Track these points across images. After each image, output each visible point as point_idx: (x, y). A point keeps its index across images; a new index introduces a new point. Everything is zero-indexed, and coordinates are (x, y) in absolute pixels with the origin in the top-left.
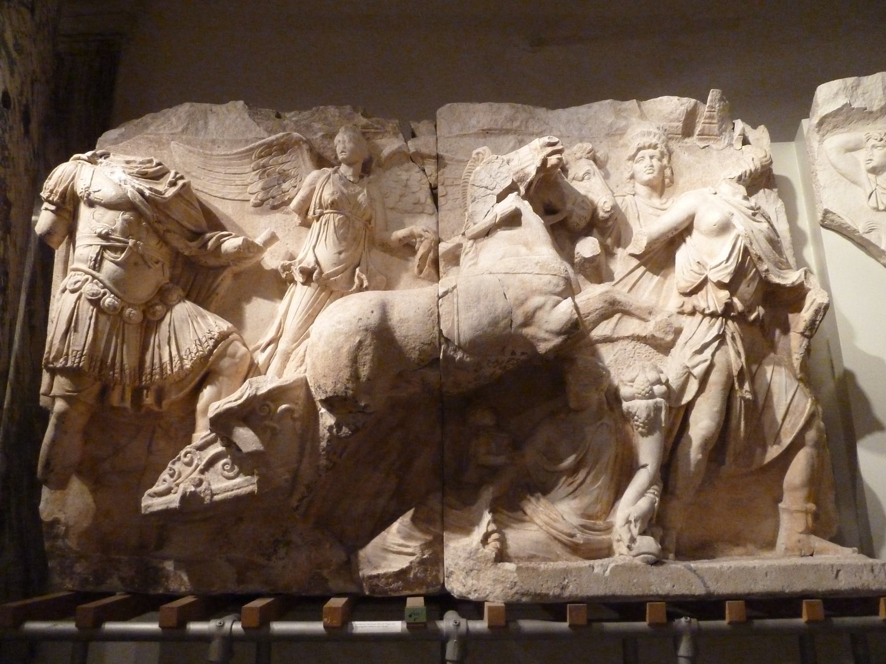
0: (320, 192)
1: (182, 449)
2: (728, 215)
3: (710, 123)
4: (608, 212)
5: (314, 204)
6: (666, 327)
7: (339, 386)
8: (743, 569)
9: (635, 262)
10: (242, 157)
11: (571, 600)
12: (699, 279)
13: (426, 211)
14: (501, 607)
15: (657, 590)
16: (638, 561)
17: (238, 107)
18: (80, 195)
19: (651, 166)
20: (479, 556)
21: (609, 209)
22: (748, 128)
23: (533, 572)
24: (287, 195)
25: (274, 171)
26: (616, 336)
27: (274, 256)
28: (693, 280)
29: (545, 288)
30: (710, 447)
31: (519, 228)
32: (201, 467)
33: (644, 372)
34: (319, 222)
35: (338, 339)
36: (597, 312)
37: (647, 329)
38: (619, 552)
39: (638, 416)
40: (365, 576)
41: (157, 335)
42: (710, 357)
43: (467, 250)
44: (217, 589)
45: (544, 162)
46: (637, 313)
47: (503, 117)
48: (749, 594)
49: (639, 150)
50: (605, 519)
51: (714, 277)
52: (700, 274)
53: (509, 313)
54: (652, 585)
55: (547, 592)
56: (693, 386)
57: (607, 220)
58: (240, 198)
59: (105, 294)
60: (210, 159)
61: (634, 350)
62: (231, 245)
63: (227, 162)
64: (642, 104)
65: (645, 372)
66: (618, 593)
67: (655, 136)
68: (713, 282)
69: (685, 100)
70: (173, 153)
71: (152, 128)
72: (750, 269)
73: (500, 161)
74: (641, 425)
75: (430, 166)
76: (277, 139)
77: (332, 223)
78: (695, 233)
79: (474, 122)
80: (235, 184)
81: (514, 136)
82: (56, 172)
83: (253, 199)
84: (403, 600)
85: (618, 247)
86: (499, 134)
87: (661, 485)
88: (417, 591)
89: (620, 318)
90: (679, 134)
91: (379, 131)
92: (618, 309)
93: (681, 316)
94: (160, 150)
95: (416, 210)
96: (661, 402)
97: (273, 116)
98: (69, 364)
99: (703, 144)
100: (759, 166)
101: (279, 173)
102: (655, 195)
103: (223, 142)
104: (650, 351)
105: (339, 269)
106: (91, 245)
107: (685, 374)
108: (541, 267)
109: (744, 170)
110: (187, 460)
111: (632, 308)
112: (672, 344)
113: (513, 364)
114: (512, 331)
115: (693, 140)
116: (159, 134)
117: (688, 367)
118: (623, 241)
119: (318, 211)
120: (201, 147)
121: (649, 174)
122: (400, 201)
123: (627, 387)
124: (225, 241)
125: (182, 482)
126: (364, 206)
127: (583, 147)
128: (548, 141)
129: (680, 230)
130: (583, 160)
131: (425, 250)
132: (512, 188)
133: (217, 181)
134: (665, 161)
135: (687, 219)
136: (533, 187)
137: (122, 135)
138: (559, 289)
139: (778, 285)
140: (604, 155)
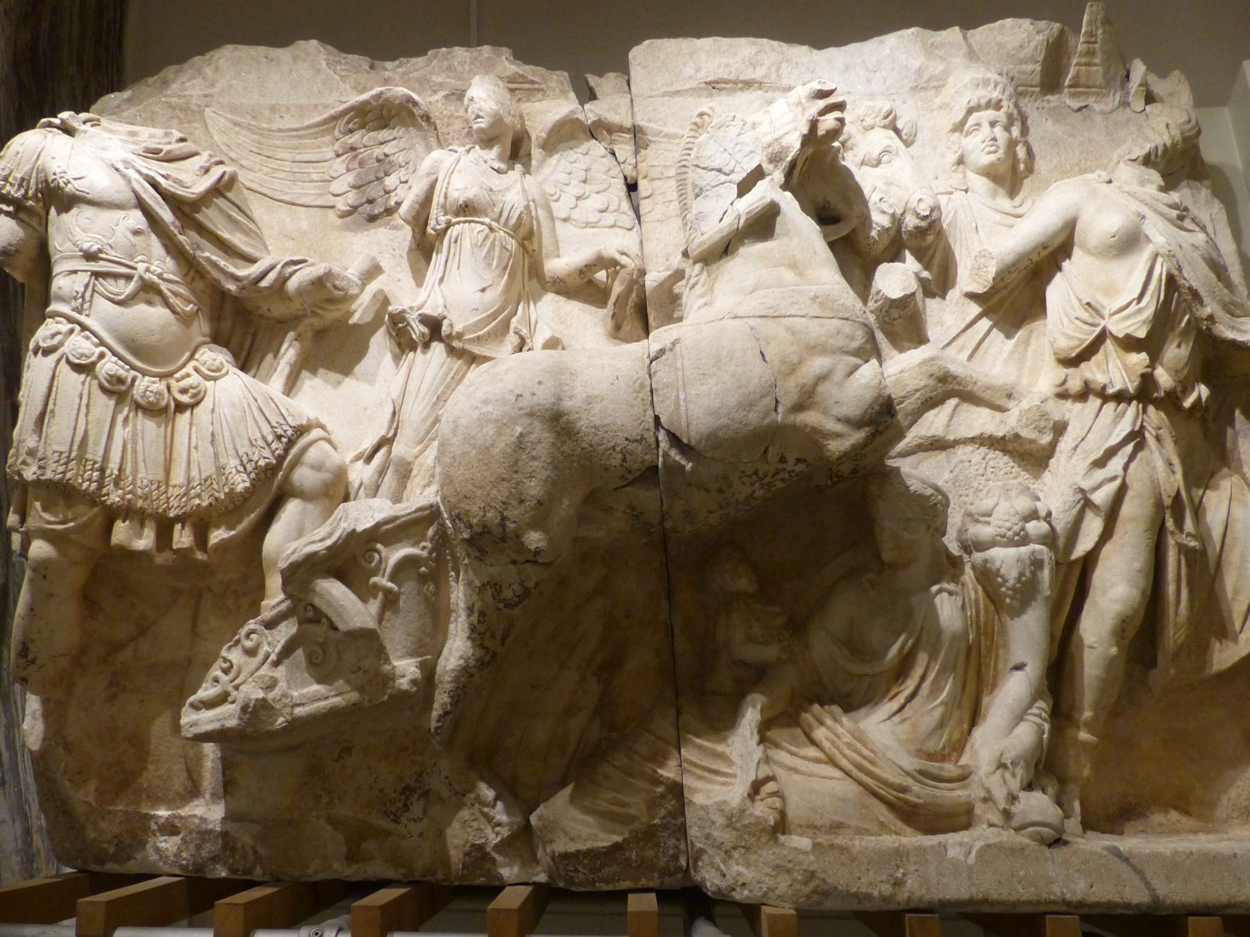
1: (242, 626)
2: (1135, 218)
3: (1088, 65)
6: (1040, 420)
8: (1215, 857)
9: (975, 309)
10: (317, 133)
11: (912, 905)
12: (1090, 334)
14: (791, 915)
15: (1062, 892)
16: (1022, 839)
20: (746, 822)
22: (1152, 78)
23: (842, 854)
26: (951, 437)
29: (831, 341)
30: (1130, 634)
32: (273, 657)
33: (1009, 499)
36: (918, 395)
38: (988, 821)
40: (735, 812)
42: (1121, 472)
43: (692, 281)
44: (315, 871)
45: (814, 125)
46: (986, 395)
48: (1227, 906)
49: (970, 111)
50: (957, 761)
51: (1119, 328)
52: (1092, 325)
53: (771, 386)
54: (1053, 883)
55: (870, 890)
56: (1093, 527)
58: (318, 203)
59: (102, 356)
63: (295, 142)
64: (969, 35)
65: (1010, 498)
66: (995, 896)
67: (996, 87)
68: (1115, 338)
69: (1042, 24)
71: (174, 86)
72: (1179, 316)
75: (623, 146)
77: (468, 240)
78: (1077, 252)
79: (689, 70)
83: (342, 205)
84: (622, 896)
86: (733, 91)
87: (1051, 702)
88: (643, 882)
89: (957, 406)
92: (953, 390)
94: (189, 123)
96: (1041, 552)
99: (1076, 104)
100: (1178, 137)
102: (1001, 191)
103: (288, 109)
106: (75, 272)
107: (1078, 502)
108: (822, 305)
109: (1153, 145)
110: (248, 644)
112: (1051, 450)
113: (783, 480)
114: (779, 419)
117: (1082, 491)
120: (254, 117)
121: (990, 153)
122: (577, 206)
124: (295, 271)
125: (243, 683)
126: (518, 212)
127: (875, 107)
128: (819, 87)
129: (1050, 249)
131: (622, 288)
133: (282, 175)
134: (1016, 131)
135: (1063, 228)
136: (796, 172)
137: (129, 100)
138: (855, 345)
139: (1233, 343)
140: (910, 124)
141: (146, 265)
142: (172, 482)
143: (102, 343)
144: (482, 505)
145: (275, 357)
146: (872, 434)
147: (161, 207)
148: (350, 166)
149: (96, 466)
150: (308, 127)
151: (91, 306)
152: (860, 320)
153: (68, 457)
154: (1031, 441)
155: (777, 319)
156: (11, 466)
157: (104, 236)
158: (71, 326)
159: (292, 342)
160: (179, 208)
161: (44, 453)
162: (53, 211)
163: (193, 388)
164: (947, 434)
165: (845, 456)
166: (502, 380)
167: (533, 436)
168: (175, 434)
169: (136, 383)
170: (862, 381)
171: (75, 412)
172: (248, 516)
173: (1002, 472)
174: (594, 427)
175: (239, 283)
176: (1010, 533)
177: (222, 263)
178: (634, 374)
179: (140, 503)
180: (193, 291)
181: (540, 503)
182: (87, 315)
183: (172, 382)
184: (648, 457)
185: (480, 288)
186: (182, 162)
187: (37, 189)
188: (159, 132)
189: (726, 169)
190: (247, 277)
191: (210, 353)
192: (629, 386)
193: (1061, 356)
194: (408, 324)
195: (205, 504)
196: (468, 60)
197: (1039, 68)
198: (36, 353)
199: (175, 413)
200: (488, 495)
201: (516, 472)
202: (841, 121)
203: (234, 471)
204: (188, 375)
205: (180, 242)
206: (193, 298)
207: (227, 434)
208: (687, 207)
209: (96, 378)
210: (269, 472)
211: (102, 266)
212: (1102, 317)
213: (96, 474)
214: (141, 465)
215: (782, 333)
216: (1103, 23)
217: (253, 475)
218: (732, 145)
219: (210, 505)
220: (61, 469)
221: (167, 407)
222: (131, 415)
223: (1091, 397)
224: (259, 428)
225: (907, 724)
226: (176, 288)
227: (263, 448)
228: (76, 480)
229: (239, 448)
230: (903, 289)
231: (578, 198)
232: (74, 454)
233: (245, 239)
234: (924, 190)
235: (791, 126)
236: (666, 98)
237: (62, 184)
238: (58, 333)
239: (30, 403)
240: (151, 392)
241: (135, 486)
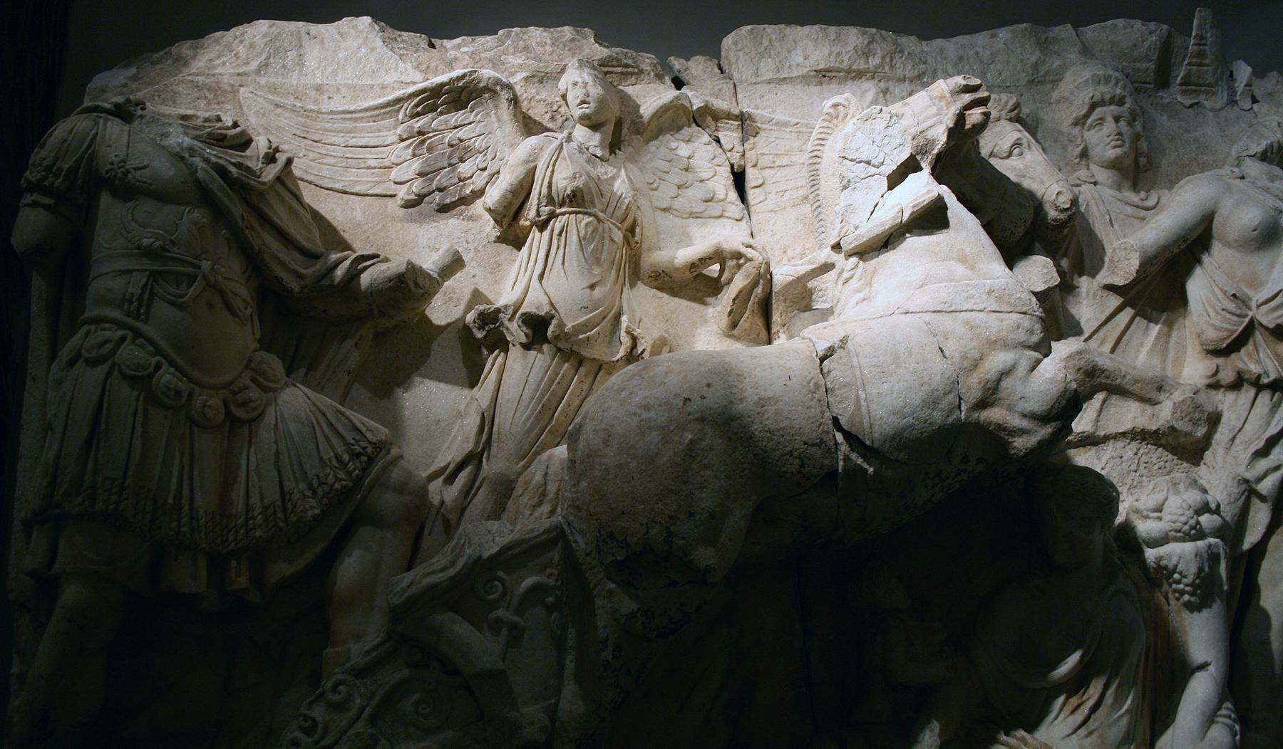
0: (548, 173)
3: (1199, 65)
4: (1066, 210)
5: (537, 196)
6: (1194, 412)
7: (655, 531)
9: (1114, 301)
10: (378, 115)
12: (1240, 325)
13: (726, 214)
17: (361, 27)
18: (107, 176)
19: (1118, 134)
21: (1068, 206)
24: (469, 185)
25: (441, 141)
26: (1102, 433)
27: (450, 299)
28: (1230, 327)
29: (1011, 336)
31: (946, 231)
33: (1177, 492)
34: (546, 233)
35: (647, 439)
37: (1163, 414)
39: (1180, 573)
41: (252, 450)
43: (846, 275)
45: (960, 118)
46: (1136, 389)
47: (851, 48)
49: (1093, 106)
52: (1239, 316)
53: (953, 383)
57: (1061, 225)
60: (315, 120)
61: (1137, 457)
62: (382, 276)
63: (349, 125)
65: (1179, 492)
68: (1266, 328)
69: (1152, 25)
70: (245, 109)
73: (885, 115)
74: (1188, 589)
75: (730, 133)
76: (451, 81)
77: (575, 231)
78: (1217, 247)
79: (797, 58)
81: (872, 82)
82: (56, 133)
83: (403, 193)
85: (1080, 276)
86: (846, 79)
89: (1104, 401)
90: (1149, 83)
91: (630, 70)
93: (1213, 392)
94: (218, 104)
95: (707, 209)
97: (424, 44)
98: (99, 506)
101: (451, 146)
102: (1127, 184)
103: (338, 90)
104: (1165, 459)
105: (594, 316)
107: (1243, 494)
108: (998, 299)
109: (1269, 142)
110: (336, 698)
111: (1125, 380)
112: (1206, 443)
115: (1175, 95)
116: (213, 75)
117: (1246, 481)
118: (1087, 263)
119: (546, 210)
123: (1149, 521)
124: (366, 268)
126: (627, 201)
128: (964, 82)
129: (1189, 242)
130: (1003, 122)
131: (746, 282)
132: (910, 166)
134: (1138, 127)
138: (1035, 338)
143: (159, 351)
144: (645, 521)
146: (1058, 429)
148: (417, 152)
150: (366, 110)
152: (1037, 313)
154: (1187, 434)
155: (953, 314)
158: (120, 333)
164: (1096, 430)
165: (1032, 452)
166: (663, 383)
167: (704, 443)
170: (1047, 375)
173: (1156, 467)
174: (769, 431)
176: (1186, 527)
178: (807, 374)
181: (712, 516)
184: (827, 462)
185: (588, 284)
189: (875, 162)
192: (804, 387)
193: (1210, 348)
194: (502, 324)
196: (549, 41)
197: (1153, 67)
200: (653, 509)
201: (685, 483)
202: (987, 115)
208: (820, 198)
212: (1250, 309)
215: (960, 329)
216: (1211, 28)
218: (880, 137)
220: (114, 498)
223: (1246, 385)
224: (331, 446)
225: (1095, 736)
230: (1046, 282)
231: (679, 187)
234: (1061, 183)
235: (935, 119)
236: (772, 85)
238: (107, 341)
240: (210, 406)
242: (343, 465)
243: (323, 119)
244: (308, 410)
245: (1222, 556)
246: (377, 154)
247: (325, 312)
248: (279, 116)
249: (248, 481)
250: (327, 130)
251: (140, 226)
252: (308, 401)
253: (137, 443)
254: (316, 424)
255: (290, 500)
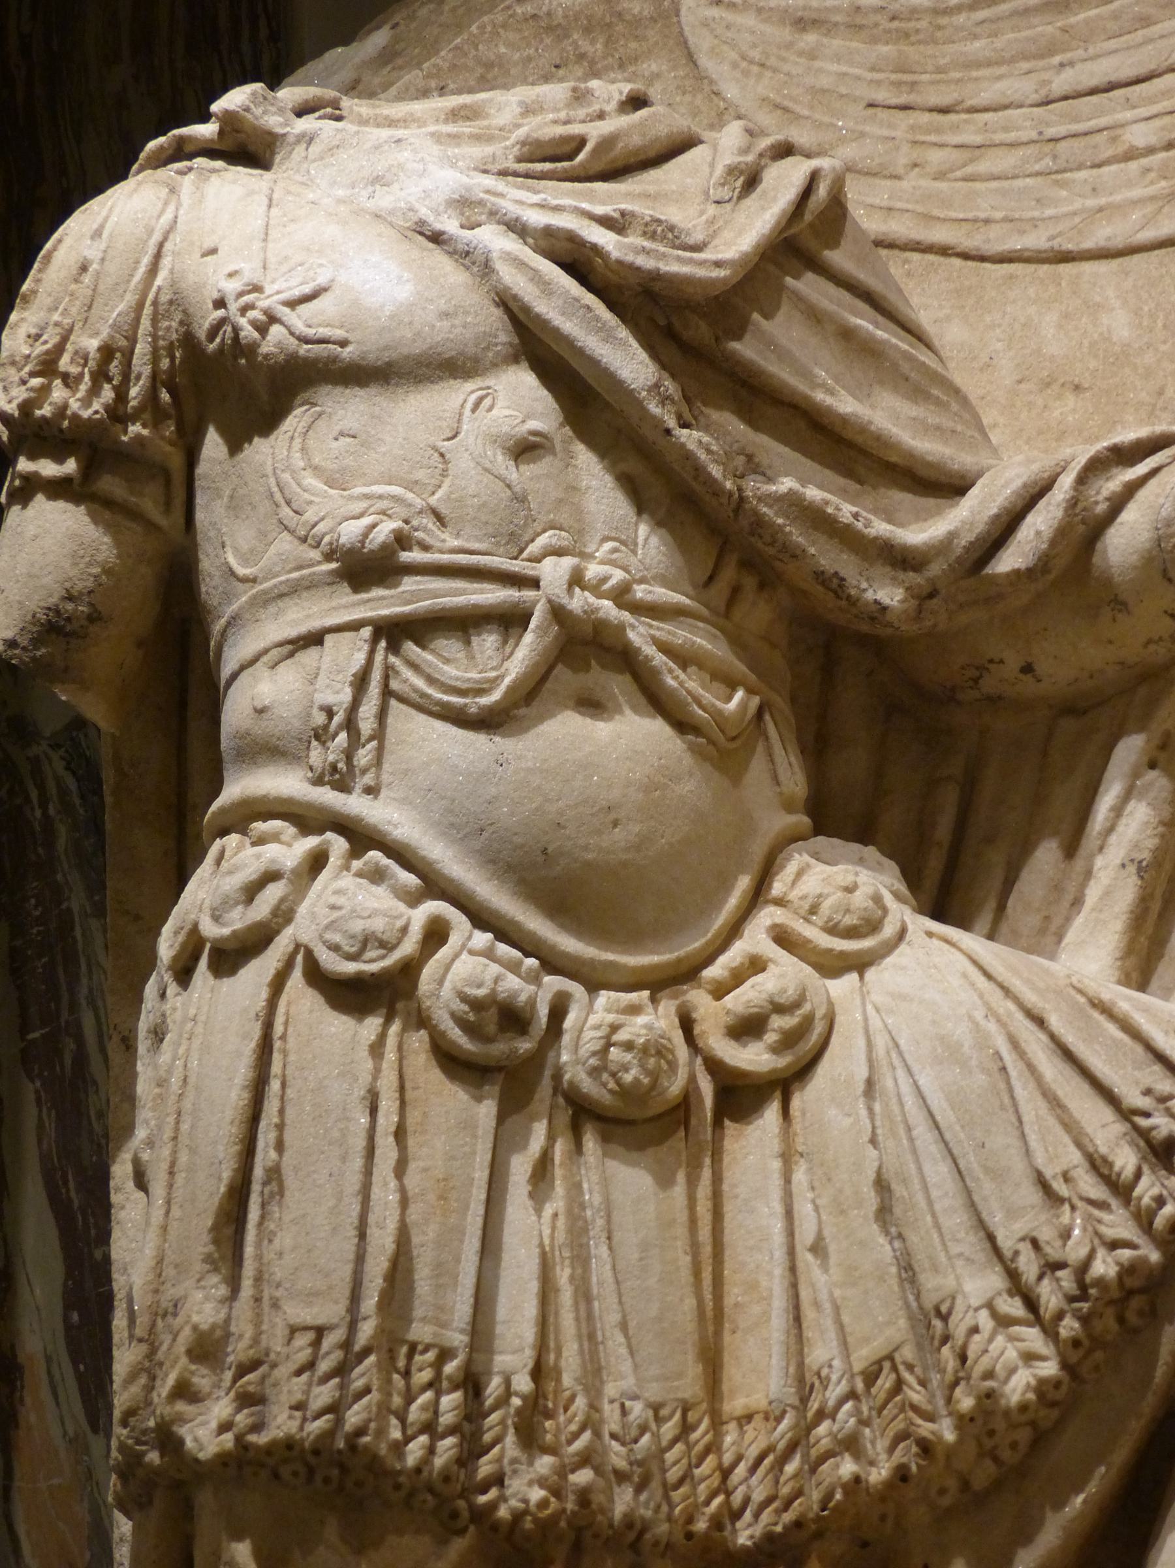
18: (212, 347)
41: (800, 1176)
59: (436, 934)
80: (1120, 149)
106: (315, 639)
124: (1131, 489)
141: (568, 562)
142: (735, 1405)
145: (1071, 849)
147: (608, 336)
149: (450, 1368)
151: (380, 750)
153: (346, 1345)
156: (130, 1413)
157: (411, 485)
159: (1136, 775)
160: (671, 334)
161: (256, 1341)
162: (213, 444)
163: (780, 1009)
168: (729, 1208)
169: (569, 1022)
171: (358, 1163)
172: (1059, 1505)
175: (912, 577)
177: (846, 511)
179: (623, 1501)
180: (736, 641)
182: (371, 791)
183: (699, 999)
186: (654, 174)
187: (154, 376)
188: (556, 92)
190: (944, 546)
191: (819, 871)
195: (879, 1474)
198: (184, 974)
199: (718, 1123)
203: (984, 1320)
204: (756, 965)
205: (688, 456)
206: (740, 668)
207: (938, 1172)
209: (421, 1020)
210: (1136, 1302)
211: (416, 596)
213: (450, 1401)
214: (615, 1344)
217: (1069, 1327)
219: (902, 1475)
220: (324, 1395)
221: (686, 1105)
222: (560, 1149)
224: (1071, 1126)
226: (680, 634)
227: (1102, 1205)
228: (381, 1432)
229: (996, 1220)
232: (366, 1330)
233: (910, 410)
237: (248, 333)
238: (270, 877)
239: (183, 1158)
240: (629, 1046)
241: (597, 1434)
242: (1122, 1190)
243: (962, 28)
244: (979, 1015)
245: (801, 489)
246: (1152, 100)
247: (1028, 669)
248: (812, 55)
249: (794, 1286)
250: (979, 64)
251: (330, 483)
252: (981, 981)
253: (385, 1194)
254: (1009, 1057)
255: (945, 1339)
